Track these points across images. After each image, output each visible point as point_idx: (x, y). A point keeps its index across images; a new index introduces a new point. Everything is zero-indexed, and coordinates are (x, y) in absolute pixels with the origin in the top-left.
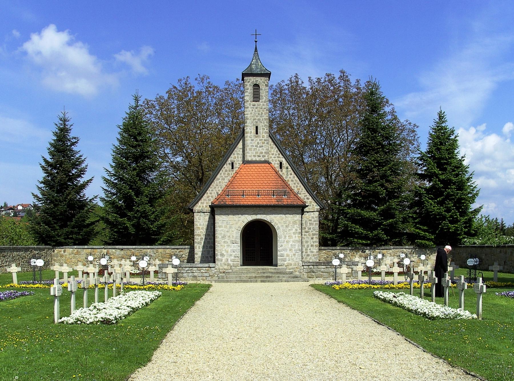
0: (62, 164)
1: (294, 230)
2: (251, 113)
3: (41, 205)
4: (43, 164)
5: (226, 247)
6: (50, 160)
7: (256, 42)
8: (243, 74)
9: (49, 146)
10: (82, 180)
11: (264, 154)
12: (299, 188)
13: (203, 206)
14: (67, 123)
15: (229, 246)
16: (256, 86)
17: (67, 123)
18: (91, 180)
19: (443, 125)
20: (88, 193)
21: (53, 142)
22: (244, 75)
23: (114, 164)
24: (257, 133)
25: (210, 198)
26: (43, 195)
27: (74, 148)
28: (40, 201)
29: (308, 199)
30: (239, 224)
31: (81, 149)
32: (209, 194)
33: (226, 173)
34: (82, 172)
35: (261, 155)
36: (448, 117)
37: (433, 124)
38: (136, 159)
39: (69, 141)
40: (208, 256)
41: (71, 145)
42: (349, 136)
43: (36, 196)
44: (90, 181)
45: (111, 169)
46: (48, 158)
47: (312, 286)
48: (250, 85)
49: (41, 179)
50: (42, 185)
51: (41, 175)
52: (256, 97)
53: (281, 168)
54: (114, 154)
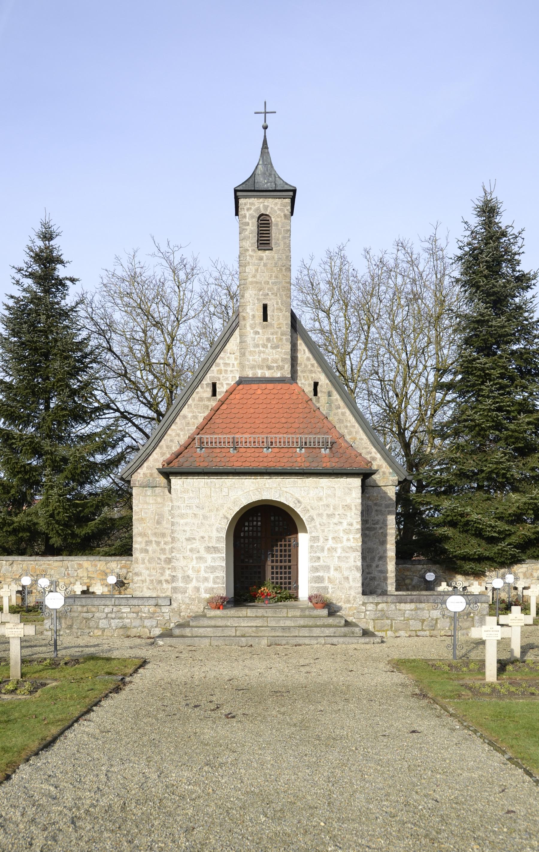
1: (345, 526)
5: (195, 561)
7: (265, 128)
8: (236, 191)
24: (265, 319)
30: (223, 512)
48: (252, 217)
53: (316, 394)
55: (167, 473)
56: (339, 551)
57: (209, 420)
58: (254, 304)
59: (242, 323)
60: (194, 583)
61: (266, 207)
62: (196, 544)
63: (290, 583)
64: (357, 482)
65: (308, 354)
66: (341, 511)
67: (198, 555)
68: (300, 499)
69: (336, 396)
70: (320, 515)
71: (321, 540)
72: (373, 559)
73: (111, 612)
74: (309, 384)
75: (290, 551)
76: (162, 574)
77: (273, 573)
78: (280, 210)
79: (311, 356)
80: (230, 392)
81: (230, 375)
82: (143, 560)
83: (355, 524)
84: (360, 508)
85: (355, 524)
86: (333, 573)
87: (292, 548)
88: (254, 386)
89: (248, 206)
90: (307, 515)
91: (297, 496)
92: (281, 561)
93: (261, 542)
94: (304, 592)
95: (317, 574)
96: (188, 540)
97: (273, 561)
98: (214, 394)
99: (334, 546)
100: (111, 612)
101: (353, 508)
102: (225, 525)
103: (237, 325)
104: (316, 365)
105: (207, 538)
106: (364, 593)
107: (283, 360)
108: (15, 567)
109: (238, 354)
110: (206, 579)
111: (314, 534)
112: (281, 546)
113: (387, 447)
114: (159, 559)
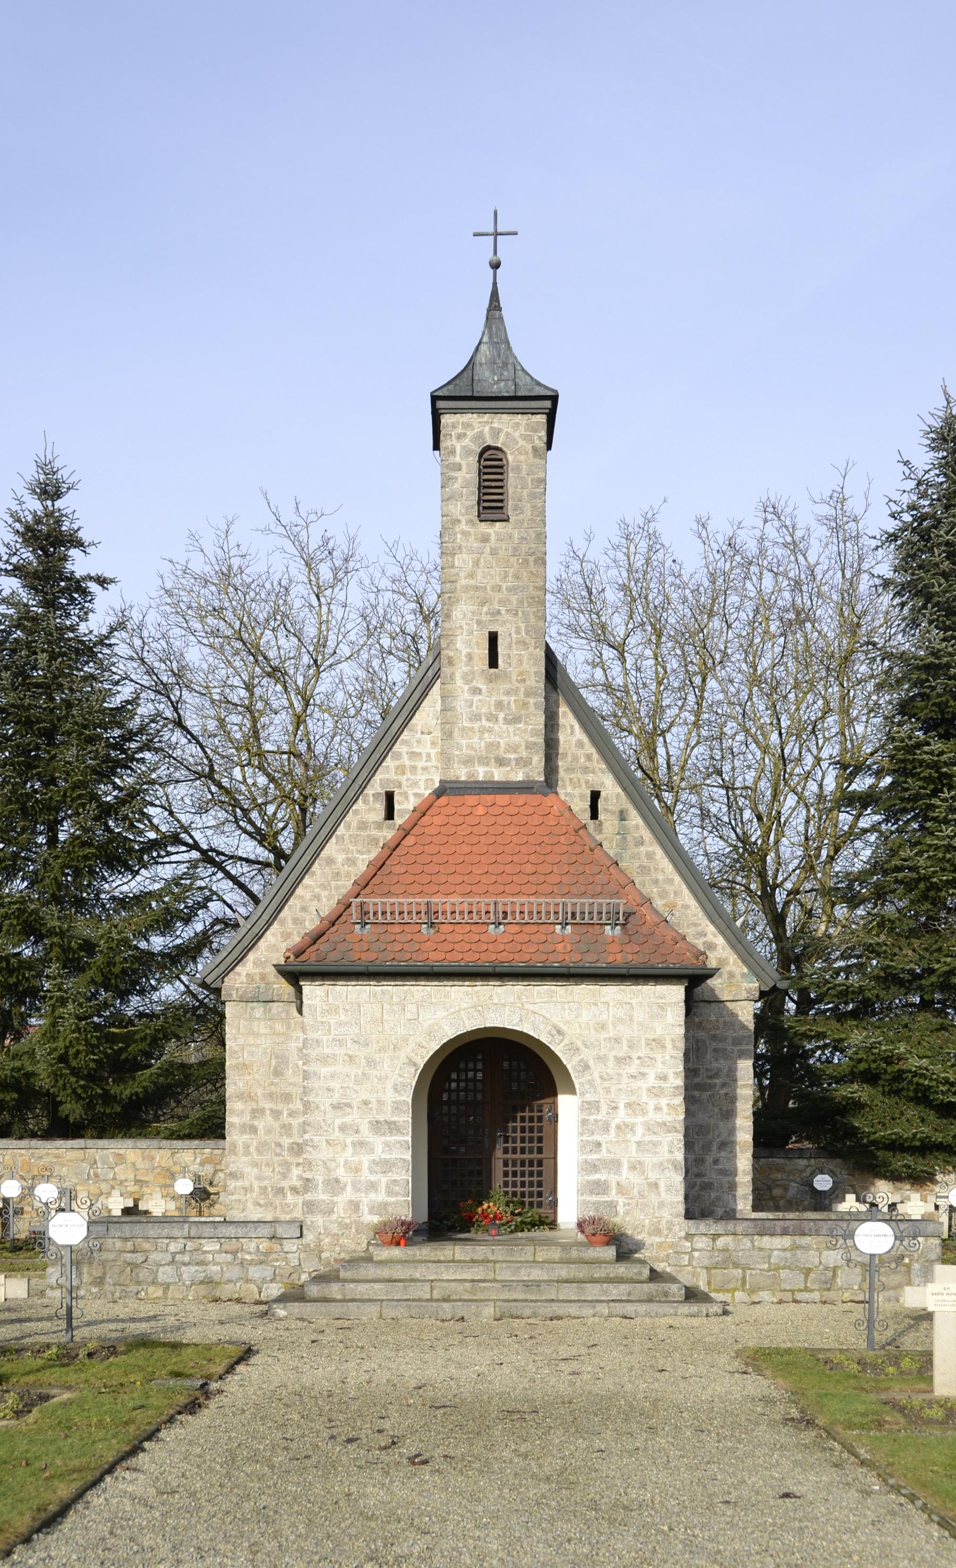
5: (350, 1150)
8: (434, 399)
15: (361, 1144)
22: (439, 403)
24: (493, 662)
53: (594, 815)
55: (295, 975)
56: (640, 1130)
57: (379, 866)
58: (471, 633)
60: (348, 1194)
61: (496, 433)
64: (676, 993)
66: (643, 1051)
67: (355, 1138)
69: (635, 819)
70: (601, 1059)
71: (604, 1108)
73: (183, 1252)
74: (582, 796)
75: (540, 1130)
76: (284, 1176)
77: (506, 1174)
78: (524, 437)
79: (585, 739)
80: (422, 812)
82: (247, 1147)
83: (671, 1077)
84: (681, 1045)
88: (471, 800)
90: (576, 1059)
91: (556, 1020)
92: (523, 1151)
93: (483, 1117)
96: (337, 1107)
97: (506, 1151)
99: (628, 1120)
100: (183, 1252)
101: (669, 1045)
102: (411, 1078)
103: (437, 676)
104: (596, 756)
105: (374, 1105)
106: (689, 1215)
107: (529, 746)
109: (438, 733)
110: (373, 1186)
111: (588, 1097)
114: (279, 1145)
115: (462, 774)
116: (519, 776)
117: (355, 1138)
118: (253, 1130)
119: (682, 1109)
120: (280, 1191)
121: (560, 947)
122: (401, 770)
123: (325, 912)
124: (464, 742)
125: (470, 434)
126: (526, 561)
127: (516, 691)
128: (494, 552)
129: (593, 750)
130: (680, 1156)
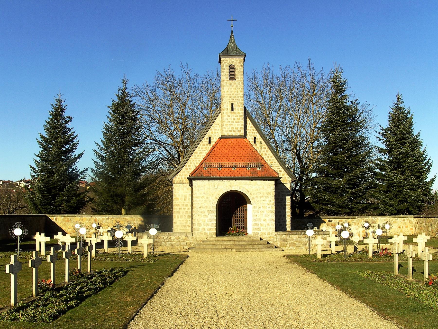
0: (58, 141)
2: (228, 92)
3: (36, 176)
4: (40, 139)
5: (203, 217)
6: (46, 136)
8: (219, 55)
9: (46, 124)
10: (74, 155)
11: (239, 129)
12: (272, 161)
13: (182, 178)
14: (62, 104)
16: (232, 68)
17: (62, 104)
18: (82, 154)
19: (401, 105)
20: (80, 166)
21: (49, 120)
23: (104, 140)
24: (232, 110)
25: (189, 170)
26: (38, 166)
27: (68, 126)
28: (36, 173)
29: (280, 171)
31: (75, 127)
32: (187, 167)
33: (204, 147)
34: (74, 147)
35: (237, 130)
36: (404, 99)
37: (392, 105)
38: (123, 135)
39: (64, 119)
40: (187, 225)
41: (65, 123)
42: (319, 112)
43: (32, 168)
44: (81, 155)
45: (101, 144)
46: (45, 134)
47: (288, 256)
48: (227, 66)
49: (38, 153)
50: (39, 159)
51: (38, 149)
52: (232, 77)
53: (255, 143)
54: (104, 130)
55: (191, 180)
56: (265, 212)
57: (208, 155)
58: (227, 103)
59: (222, 112)
61: (233, 62)
62: (203, 210)
63: (243, 227)
64: (273, 183)
65: (251, 125)
66: (266, 195)
67: (204, 214)
68: (249, 190)
69: (263, 143)
71: (258, 207)
72: (280, 216)
73: (167, 239)
74: (252, 138)
75: (243, 212)
76: (186, 223)
77: (236, 222)
78: (239, 63)
79: (253, 126)
80: (217, 143)
81: (217, 134)
82: (178, 216)
83: (272, 201)
84: (274, 194)
85: (272, 201)
86: (262, 222)
87: (244, 211)
88: (228, 140)
89: (225, 61)
90: (251, 197)
91: (247, 188)
92: (240, 217)
93: (231, 210)
94: (250, 230)
95: (255, 222)
96: (200, 207)
97: (236, 217)
98: (210, 142)
99: (263, 210)
100: (167, 239)
101: (271, 194)
102: (216, 201)
103: (220, 112)
104: (255, 129)
105: (208, 207)
106: (276, 231)
107: (240, 128)
108: (109, 220)
109: (220, 125)
110: (208, 225)
111: (254, 205)
112: (239, 210)
113: (287, 166)
114: (185, 216)
115: (226, 134)
116: (238, 134)
117: (204, 214)
118: (179, 212)
119: (274, 208)
120: (185, 226)
121: (248, 173)
122: (212, 133)
123: (197, 165)
124: (226, 127)
125: (227, 62)
126: (239, 89)
127: (237, 116)
128: (232, 86)
129: (254, 128)
130: (274, 218)
